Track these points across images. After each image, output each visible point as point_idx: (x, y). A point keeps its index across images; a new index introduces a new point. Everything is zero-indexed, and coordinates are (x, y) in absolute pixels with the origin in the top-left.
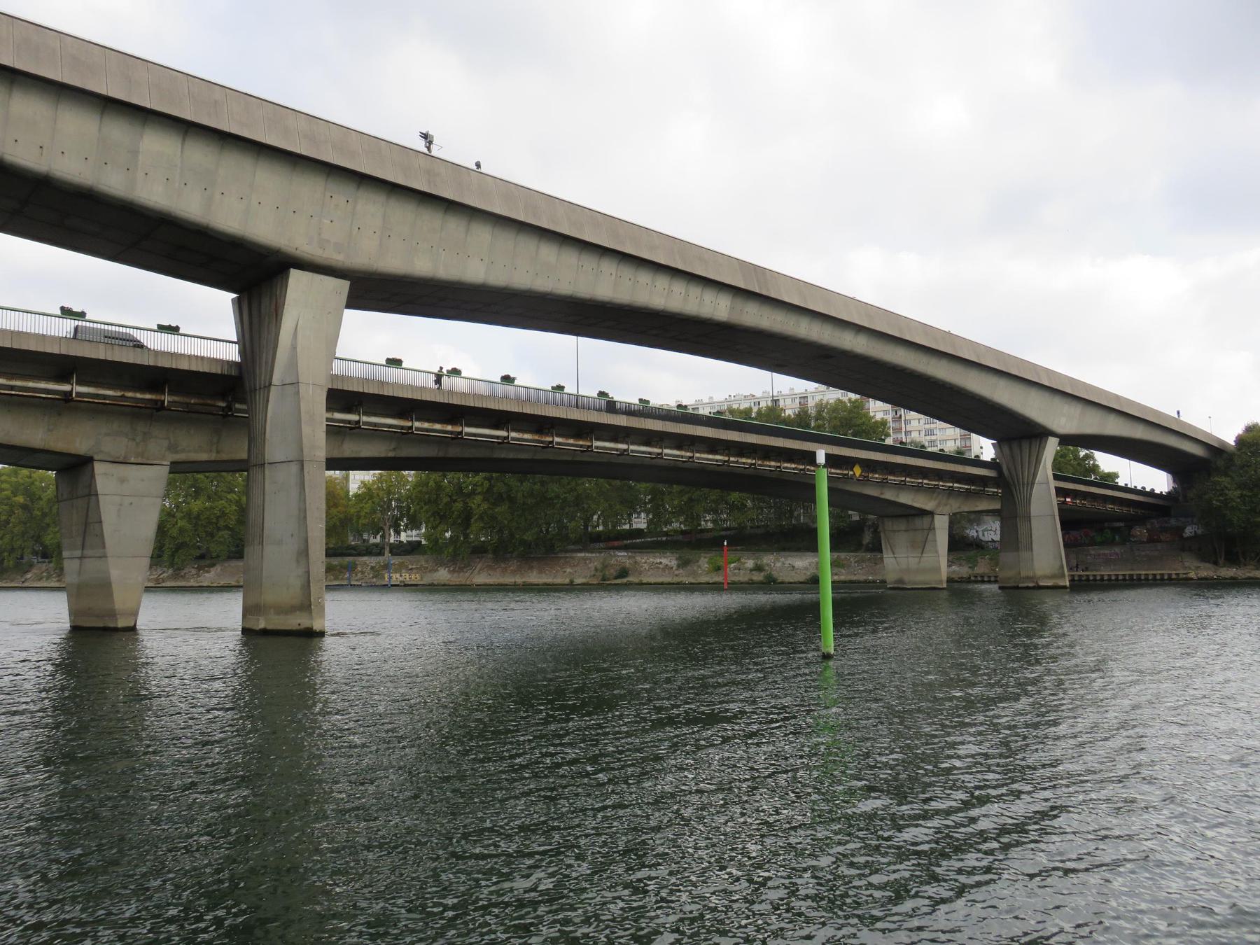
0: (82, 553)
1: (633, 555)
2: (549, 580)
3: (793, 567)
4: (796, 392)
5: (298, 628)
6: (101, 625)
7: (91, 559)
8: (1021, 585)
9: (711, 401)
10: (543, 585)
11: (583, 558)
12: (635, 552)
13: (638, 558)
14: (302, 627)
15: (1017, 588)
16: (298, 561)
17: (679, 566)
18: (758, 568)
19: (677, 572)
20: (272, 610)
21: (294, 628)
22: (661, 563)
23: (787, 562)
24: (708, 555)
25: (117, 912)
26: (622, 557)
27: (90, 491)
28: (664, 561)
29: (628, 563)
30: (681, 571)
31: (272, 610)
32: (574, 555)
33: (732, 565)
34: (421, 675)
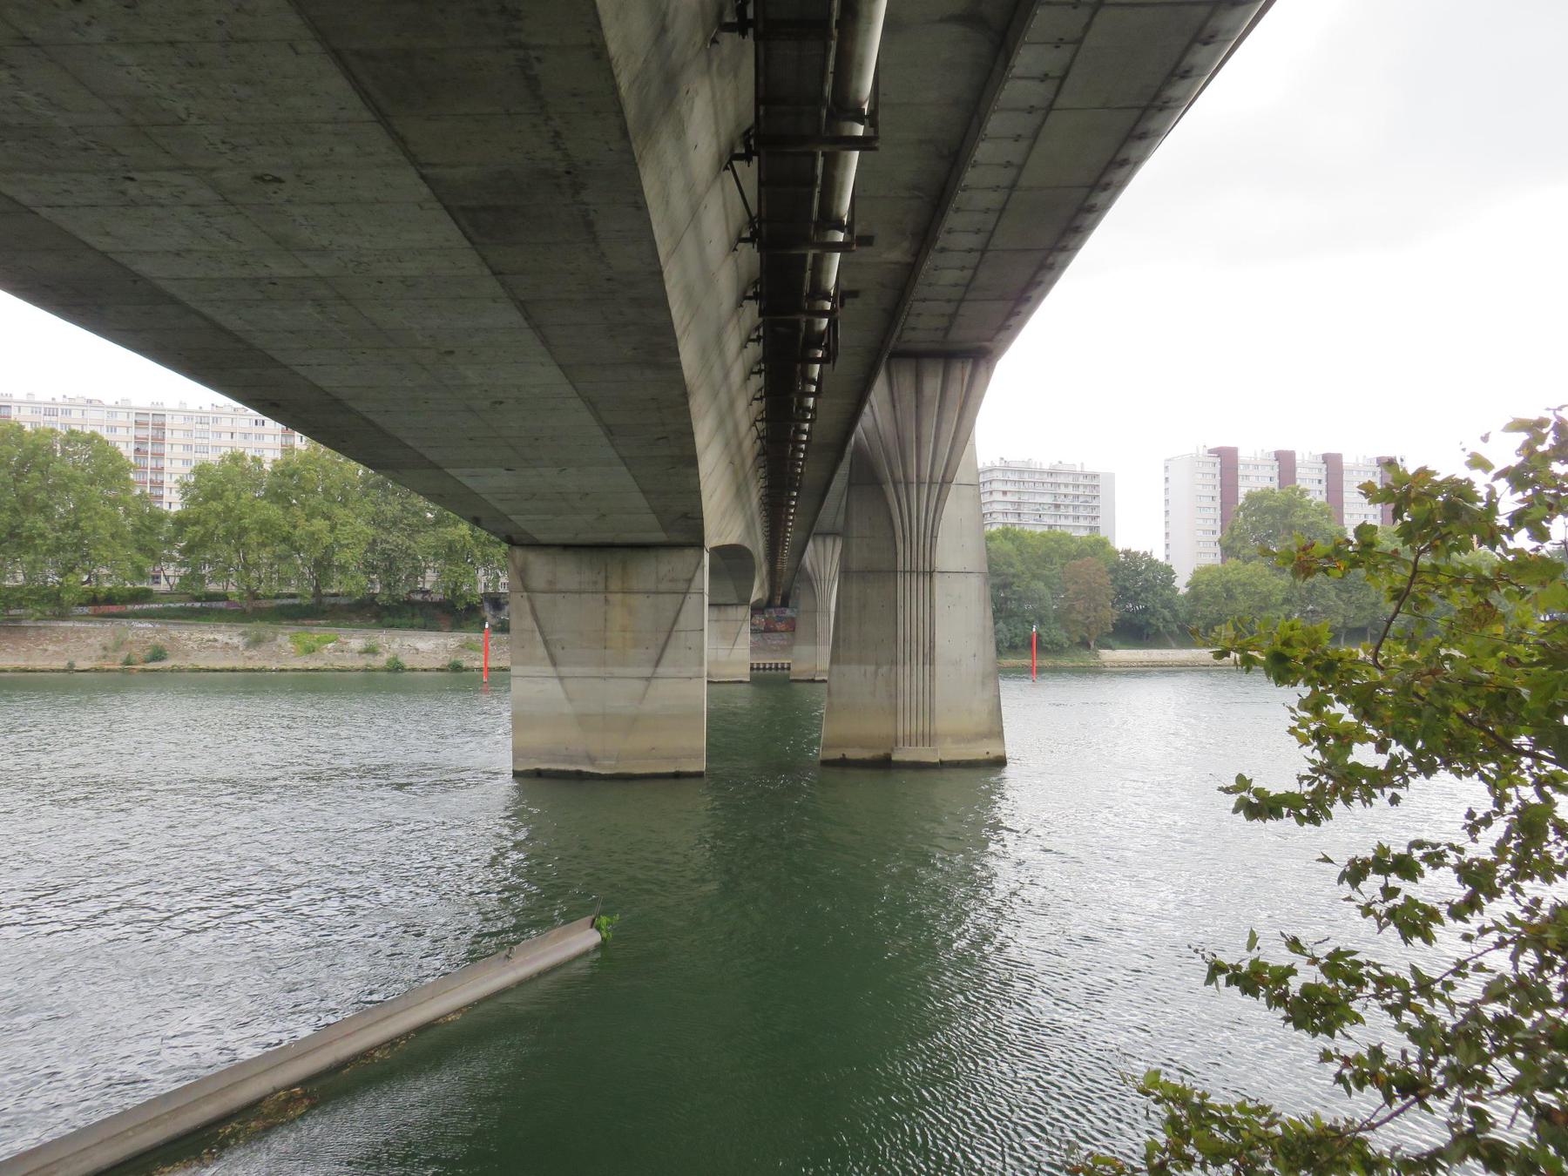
0: (654, 673)
1: (164, 627)
2: (21, 663)
3: (417, 650)
4: (133, 405)
5: (986, 757)
6: (672, 770)
7: (665, 680)
8: (817, 678)
9: (31, 399)
10: (14, 671)
11: (72, 628)
12: (167, 624)
13: (175, 633)
14: (991, 756)
15: (813, 681)
16: (983, 684)
17: (248, 646)
18: (370, 651)
19: (247, 654)
20: (949, 740)
21: (981, 758)
22: (216, 640)
23: (406, 643)
24: (288, 632)
25: (993, 1112)
26: (143, 631)
27: (689, 587)
28: (219, 637)
29: (160, 639)
30: (254, 653)
31: (949, 740)
32: (54, 624)
33: (330, 645)
34: (492, 809)
